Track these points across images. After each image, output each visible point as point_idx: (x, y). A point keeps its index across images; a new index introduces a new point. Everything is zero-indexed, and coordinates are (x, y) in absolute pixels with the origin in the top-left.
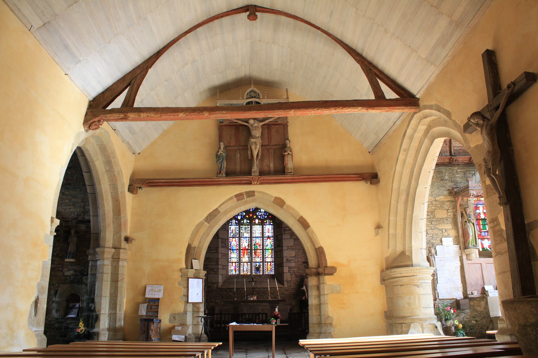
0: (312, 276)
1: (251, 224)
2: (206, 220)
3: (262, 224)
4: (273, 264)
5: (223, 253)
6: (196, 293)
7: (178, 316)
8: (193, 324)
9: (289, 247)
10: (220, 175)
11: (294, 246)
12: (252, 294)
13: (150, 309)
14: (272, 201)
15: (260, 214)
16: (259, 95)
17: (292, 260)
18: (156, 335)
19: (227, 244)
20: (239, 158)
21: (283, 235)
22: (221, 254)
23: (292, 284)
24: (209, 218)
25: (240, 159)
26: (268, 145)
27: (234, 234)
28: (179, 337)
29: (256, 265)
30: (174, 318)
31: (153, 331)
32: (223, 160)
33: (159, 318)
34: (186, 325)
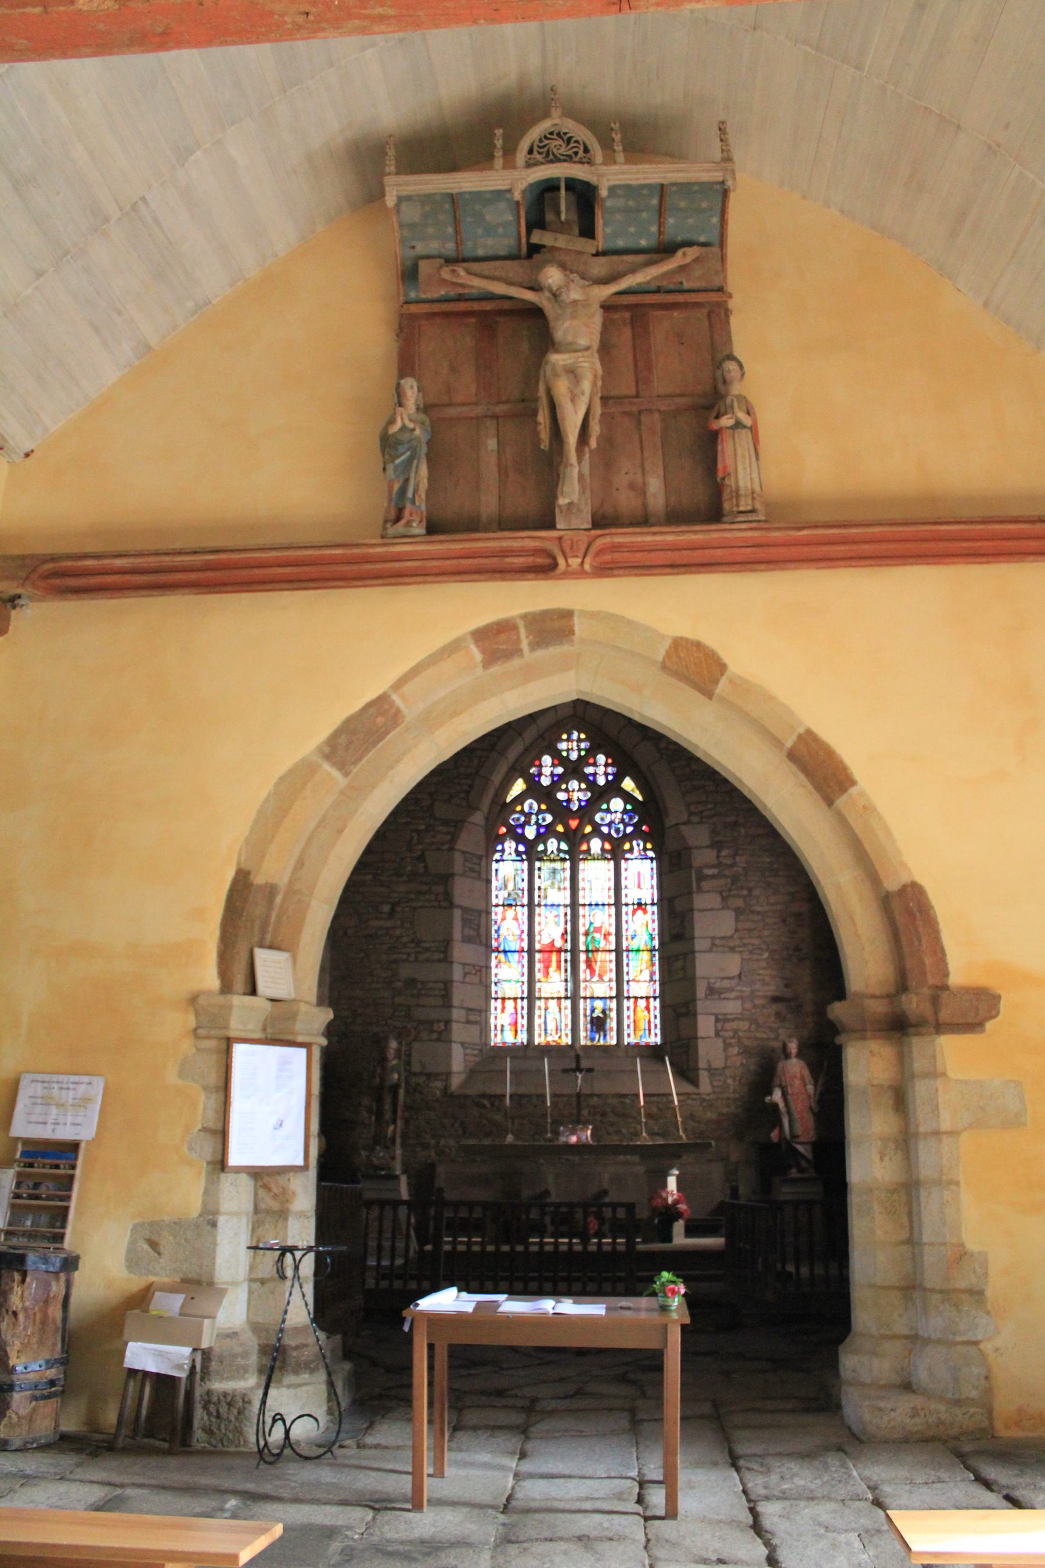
0: (864, 1038)
1: (575, 856)
2: (327, 750)
3: (616, 853)
4: (655, 1008)
5: (469, 965)
6: (273, 1121)
7: (171, 1238)
8: (253, 1276)
9: (717, 942)
10: (400, 528)
11: (736, 936)
12: (578, 1122)
13: (31, 1197)
14: (660, 658)
15: (607, 820)
16: (586, 150)
17: (731, 990)
18: (34, 1340)
19: (483, 931)
20: (495, 455)
21: (695, 895)
22: (461, 967)
23: (730, 1081)
24: (343, 740)
25: (499, 459)
26: (637, 396)
27: (509, 895)
28: (160, 1354)
29: (593, 1010)
30: (153, 1245)
31: (21, 1316)
32: (409, 462)
33: (68, 1243)
34: (211, 1284)
